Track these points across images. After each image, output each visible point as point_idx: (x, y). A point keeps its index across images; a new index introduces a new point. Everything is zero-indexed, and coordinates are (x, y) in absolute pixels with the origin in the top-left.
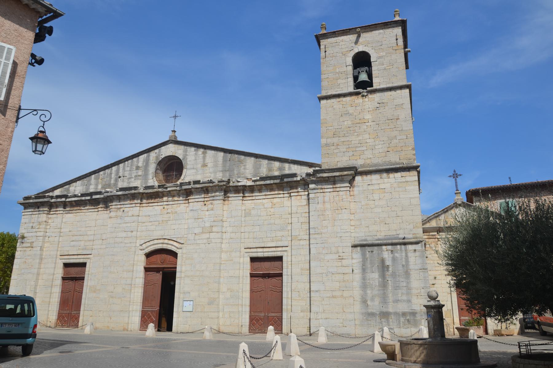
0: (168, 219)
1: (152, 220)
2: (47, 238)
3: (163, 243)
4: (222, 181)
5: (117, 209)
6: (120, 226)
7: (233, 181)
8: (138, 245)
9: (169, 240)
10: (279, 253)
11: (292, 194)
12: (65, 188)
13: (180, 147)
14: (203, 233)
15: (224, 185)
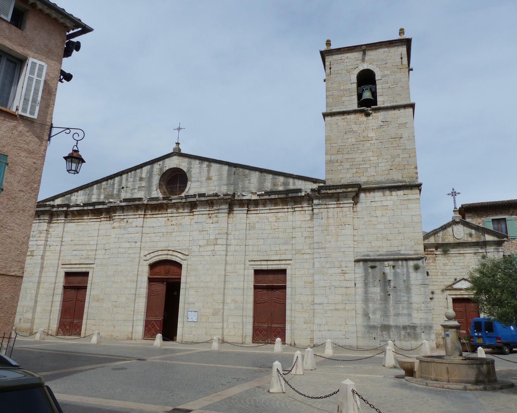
0: (172, 231)
1: (156, 231)
2: (48, 247)
3: (167, 255)
4: (227, 194)
5: (121, 219)
6: (124, 236)
7: (238, 195)
8: (142, 255)
9: (174, 251)
10: (283, 266)
14: (207, 245)
15: (229, 199)
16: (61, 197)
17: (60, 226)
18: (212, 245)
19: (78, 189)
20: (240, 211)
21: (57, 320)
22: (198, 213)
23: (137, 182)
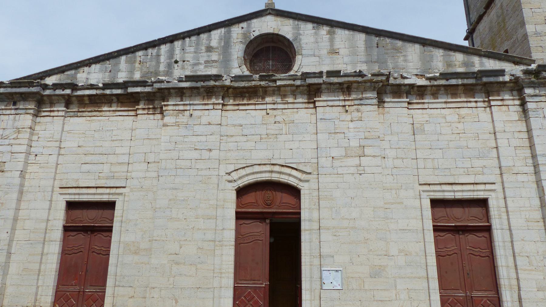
0: (277, 132)
1: (245, 132)
2: (32, 157)
3: (272, 172)
4: (379, 73)
5: (178, 111)
6: (186, 140)
7: (395, 77)
8: (222, 173)
9: (283, 166)
10: (482, 193)
11: (493, 103)
12: (67, 74)
13: (286, 21)
14: (346, 156)
15: (381, 81)
16: (56, 74)
17: (56, 121)
18: (355, 157)
19: (91, 61)
20: (396, 104)
21: (52, 287)
22: (325, 104)
23: (202, 53)
